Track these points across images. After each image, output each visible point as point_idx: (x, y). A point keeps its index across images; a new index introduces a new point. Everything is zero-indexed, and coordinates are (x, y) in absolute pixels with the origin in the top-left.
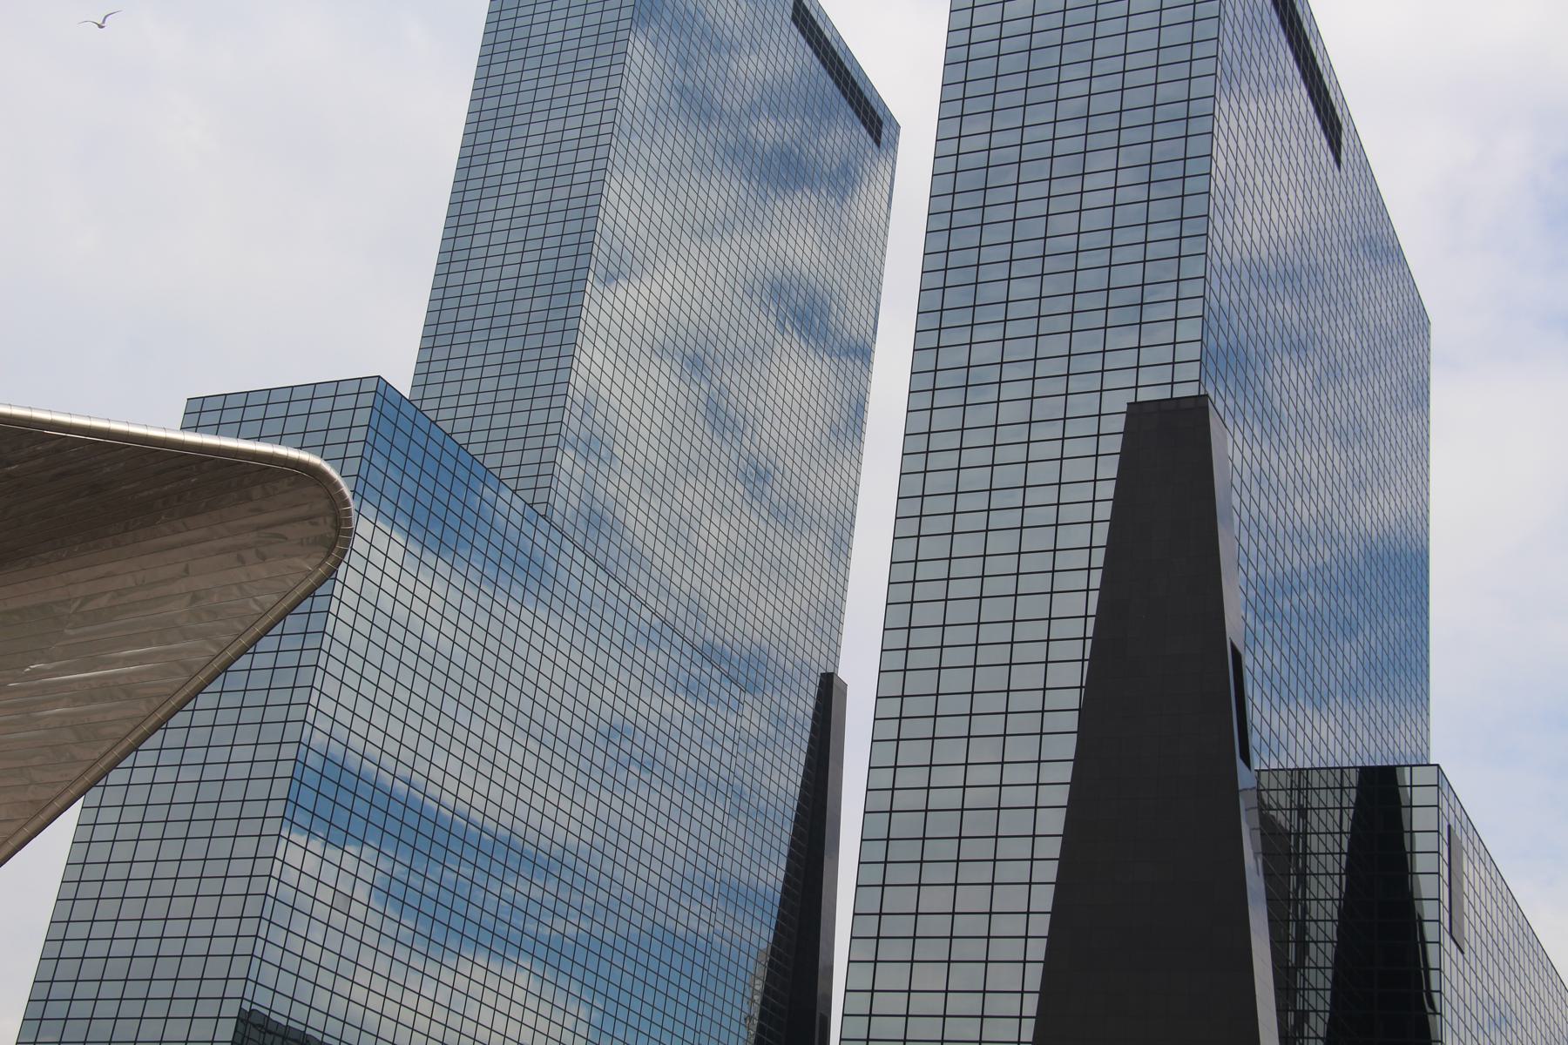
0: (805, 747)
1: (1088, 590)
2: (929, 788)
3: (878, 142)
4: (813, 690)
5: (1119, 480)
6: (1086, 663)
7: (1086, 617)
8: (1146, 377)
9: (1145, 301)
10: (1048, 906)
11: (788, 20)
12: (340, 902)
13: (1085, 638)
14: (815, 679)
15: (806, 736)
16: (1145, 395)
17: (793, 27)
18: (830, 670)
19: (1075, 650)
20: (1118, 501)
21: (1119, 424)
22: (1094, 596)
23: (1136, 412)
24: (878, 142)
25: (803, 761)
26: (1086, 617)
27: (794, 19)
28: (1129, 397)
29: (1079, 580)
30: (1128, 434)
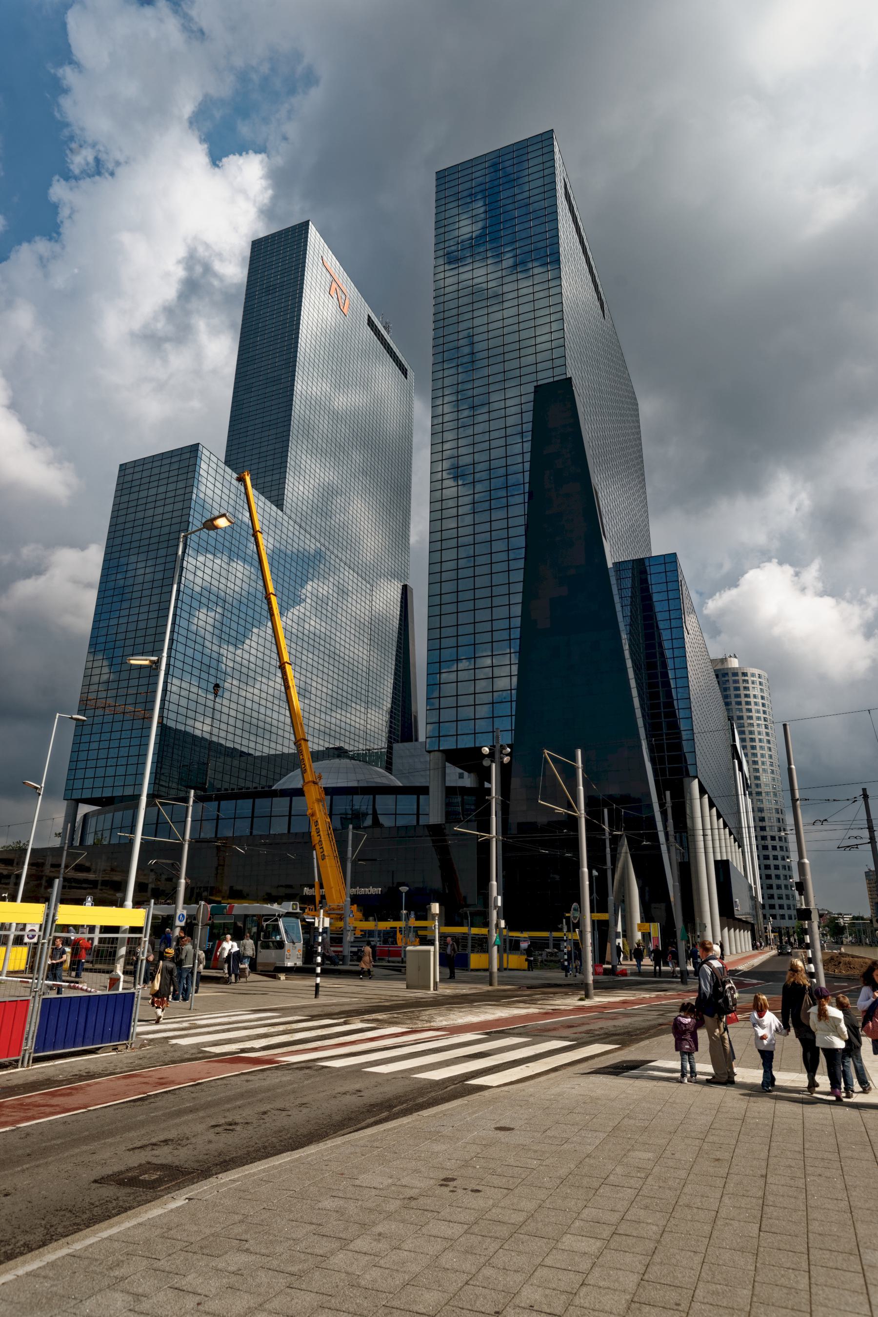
6: (514, 704)
12: (204, 668)
16: (540, 383)
26: (511, 701)
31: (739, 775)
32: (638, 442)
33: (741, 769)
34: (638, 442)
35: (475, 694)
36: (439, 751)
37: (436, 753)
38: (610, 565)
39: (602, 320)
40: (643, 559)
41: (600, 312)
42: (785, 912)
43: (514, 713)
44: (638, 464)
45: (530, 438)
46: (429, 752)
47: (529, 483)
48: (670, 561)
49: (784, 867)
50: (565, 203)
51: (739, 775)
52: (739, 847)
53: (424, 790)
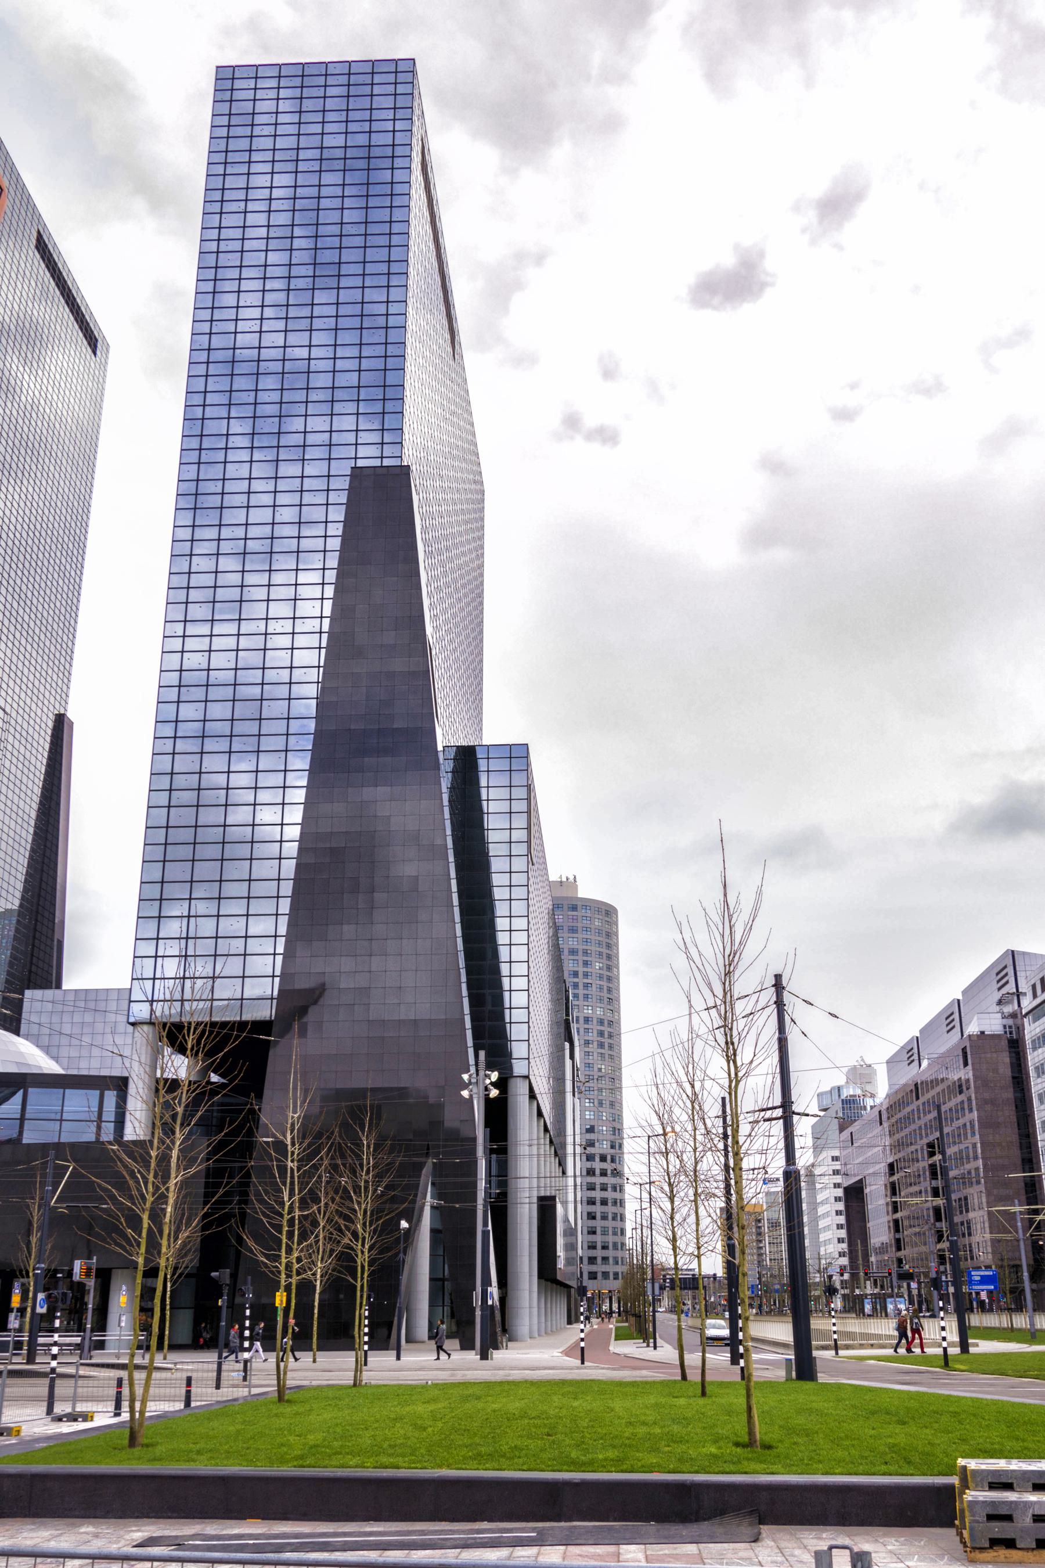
0: (45, 762)
1: (321, 633)
2: (206, 701)
3: (95, 354)
4: (50, 724)
5: (346, 523)
6: (323, 651)
7: (320, 648)
8: (362, 451)
9: (370, 194)
10: (299, 819)
11: (33, 247)
13: (319, 667)
14: (52, 717)
15: (46, 754)
16: (360, 463)
17: (36, 253)
18: (62, 712)
19: (313, 675)
20: (345, 538)
21: (345, 483)
22: (325, 636)
23: (357, 474)
24: (95, 354)
25: (43, 771)
26: (320, 648)
27: (37, 247)
28: (352, 463)
29: (267, 946)
30: (351, 490)
31: (568, 1062)
32: (479, 497)
33: (572, 1057)
34: (479, 497)
35: (366, 223)
36: (151, 1023)
37: (146, 1028)
38: (440, 748)
39: (451, 362)
40: (474, 747)
41: (450, 350)
42: (611, 1268)
43: (322, 664)
44: (476, 520)
45: (340, 532)
46: (133, 1024)
47: (331, 618)
48: (737, 247)
49: (615, 1203)
50: (421, 178)
51: (568, 1062)
52: (560, 1164)
53: (121, 1084)
